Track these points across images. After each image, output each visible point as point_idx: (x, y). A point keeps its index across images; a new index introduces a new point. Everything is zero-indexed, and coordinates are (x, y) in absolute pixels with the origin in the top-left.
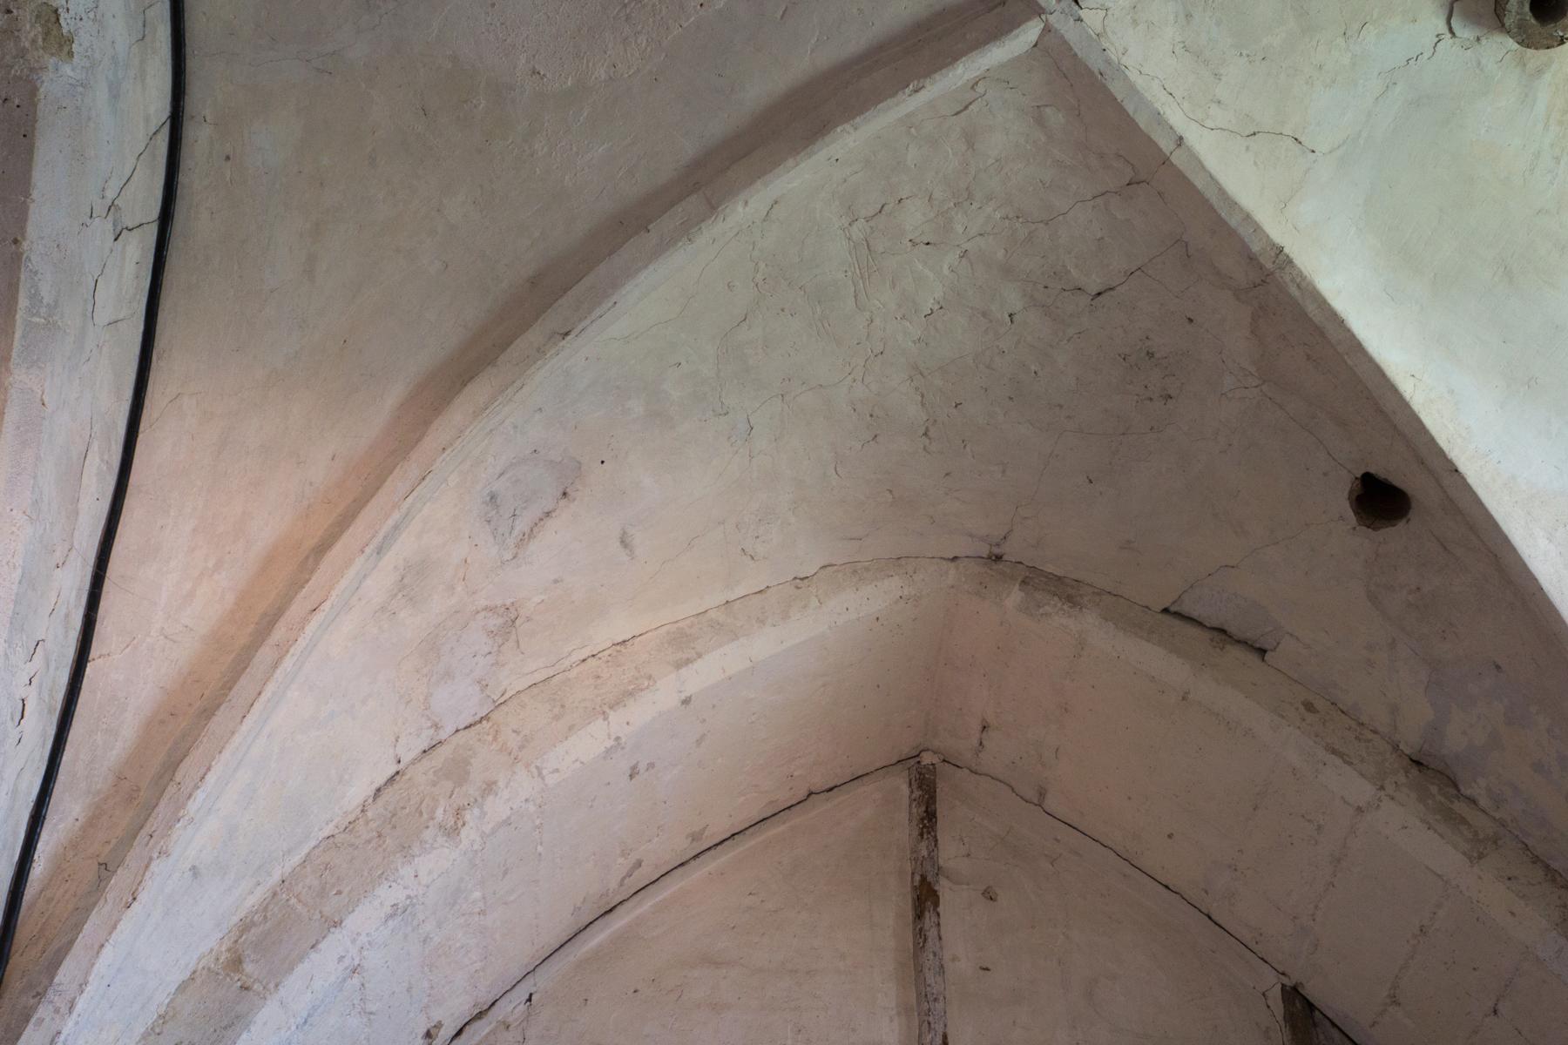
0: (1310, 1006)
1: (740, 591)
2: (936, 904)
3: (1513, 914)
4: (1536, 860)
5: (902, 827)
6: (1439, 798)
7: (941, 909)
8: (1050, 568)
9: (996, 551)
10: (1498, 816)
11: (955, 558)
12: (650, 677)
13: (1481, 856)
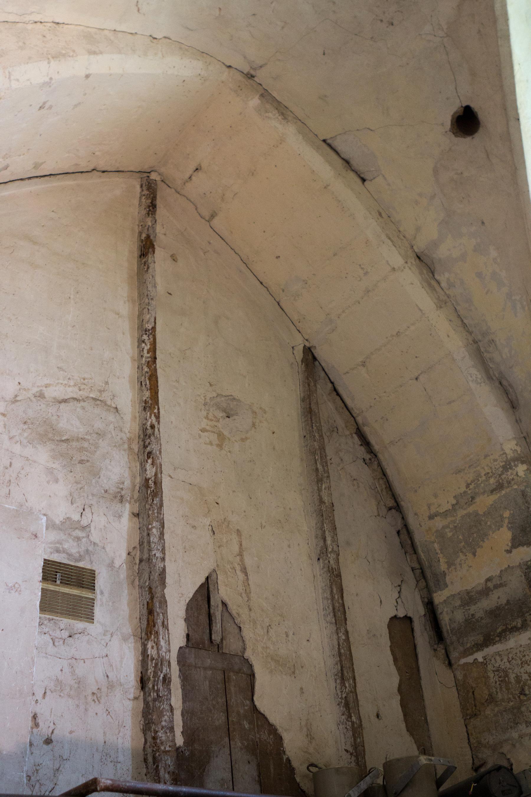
0: (315, 359)
1: (123, 28)
2: (154, 252)
3: (448, 336)
4: (459, 316)
5: (135, 208)
6: (426, 276)
7: (155, 255)
8: (275, 94)
9: (252, 72)
10: (447, 293)
11: (230, 67)
12: (74, 51)
13: (441, 307)
